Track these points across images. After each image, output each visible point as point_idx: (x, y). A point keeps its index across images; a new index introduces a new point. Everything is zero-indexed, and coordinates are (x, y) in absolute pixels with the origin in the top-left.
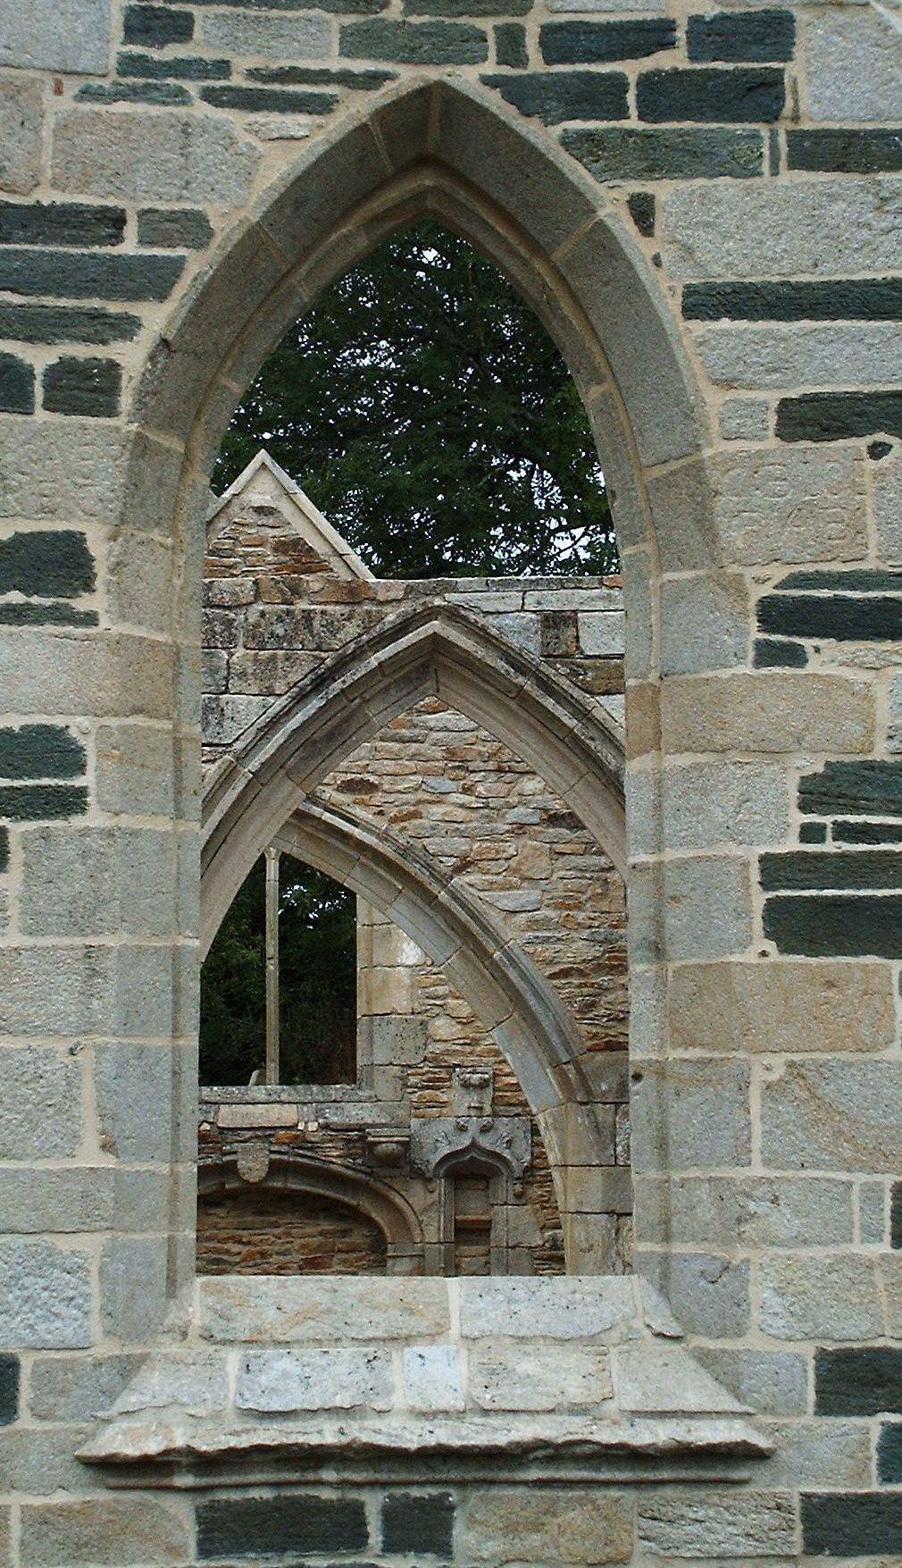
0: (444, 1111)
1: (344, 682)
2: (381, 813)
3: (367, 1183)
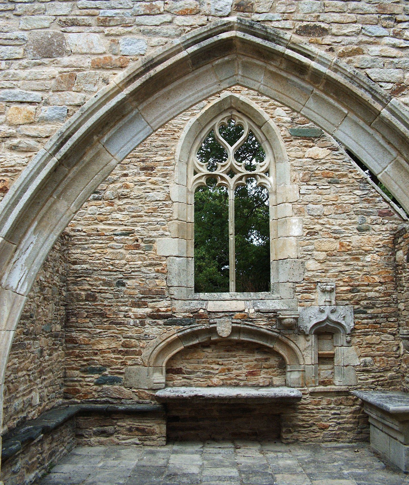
0: (313, 303)
2: (332, 50)
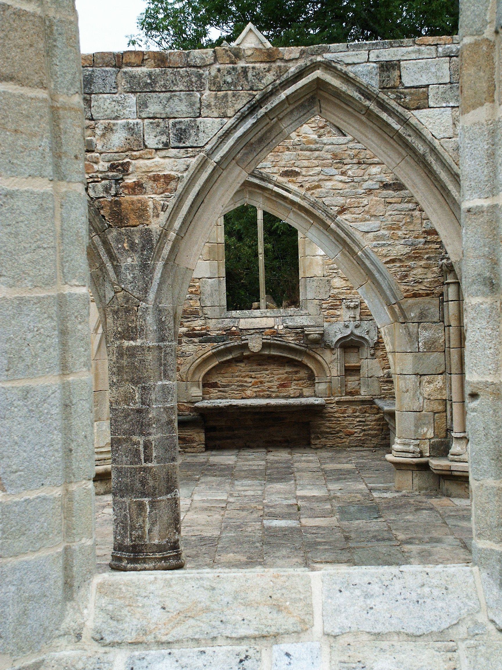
0: (339, 319)
1: (266, 108)
2: (302, 186)
3: (306, 352)
